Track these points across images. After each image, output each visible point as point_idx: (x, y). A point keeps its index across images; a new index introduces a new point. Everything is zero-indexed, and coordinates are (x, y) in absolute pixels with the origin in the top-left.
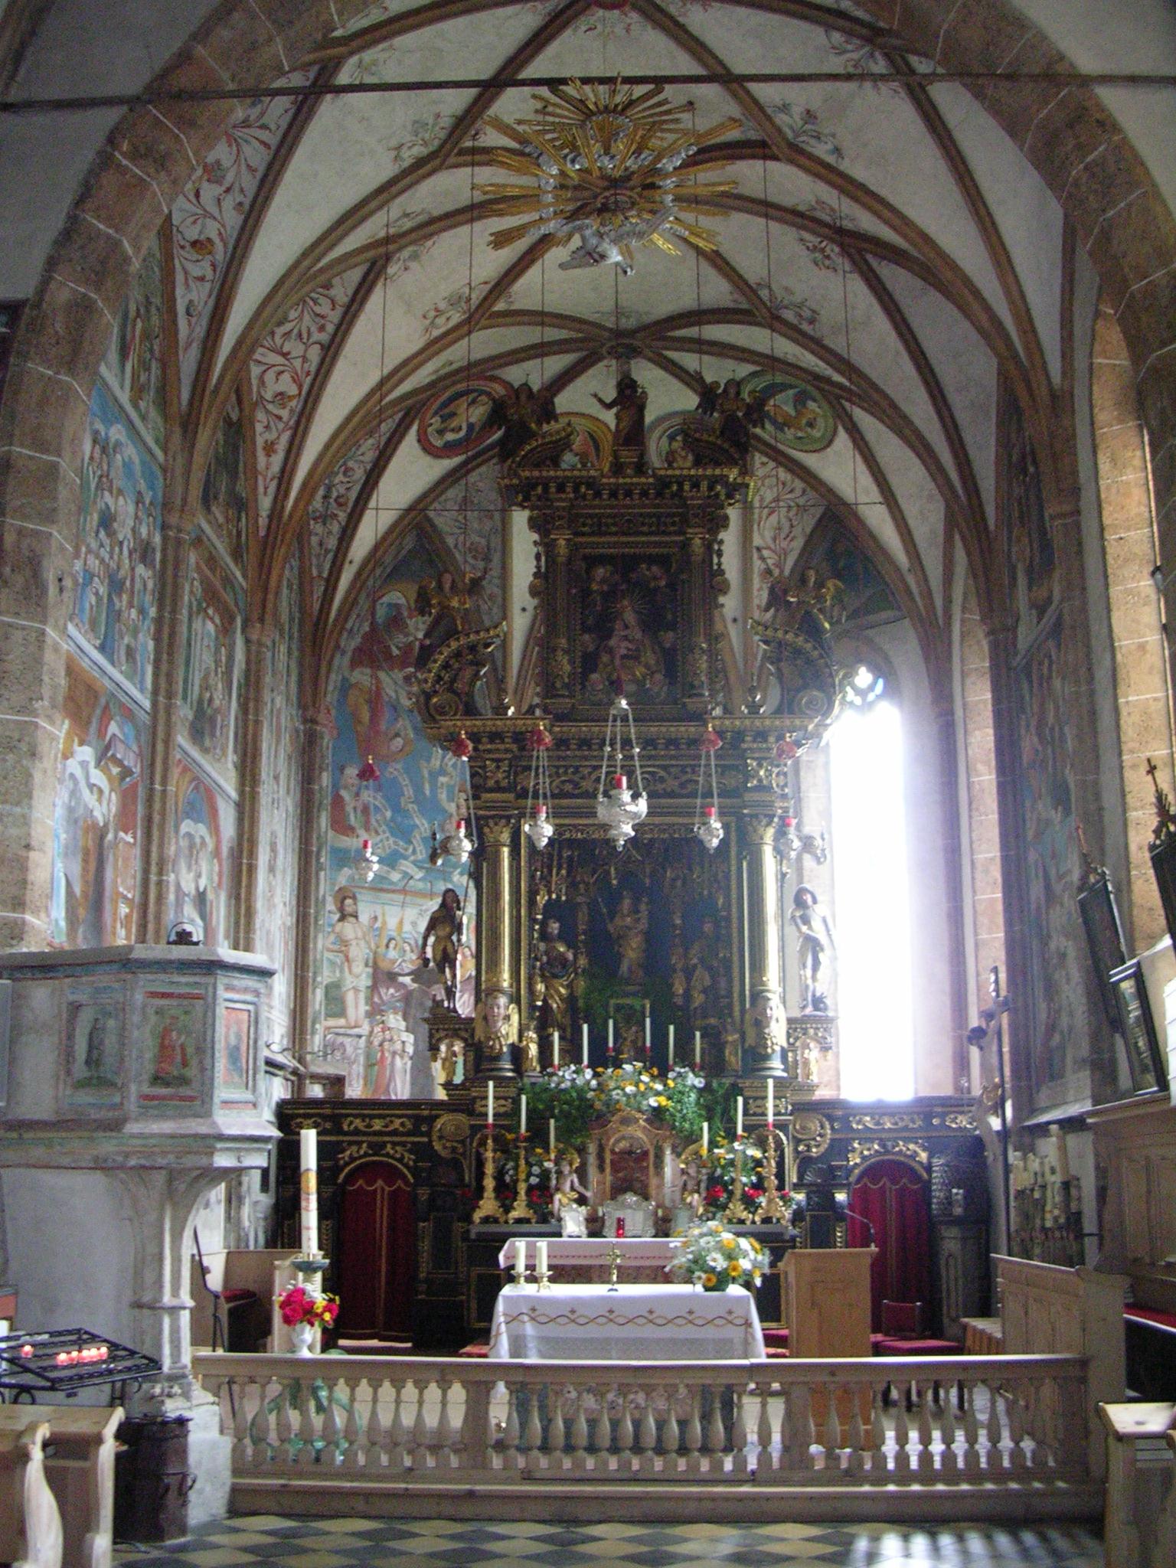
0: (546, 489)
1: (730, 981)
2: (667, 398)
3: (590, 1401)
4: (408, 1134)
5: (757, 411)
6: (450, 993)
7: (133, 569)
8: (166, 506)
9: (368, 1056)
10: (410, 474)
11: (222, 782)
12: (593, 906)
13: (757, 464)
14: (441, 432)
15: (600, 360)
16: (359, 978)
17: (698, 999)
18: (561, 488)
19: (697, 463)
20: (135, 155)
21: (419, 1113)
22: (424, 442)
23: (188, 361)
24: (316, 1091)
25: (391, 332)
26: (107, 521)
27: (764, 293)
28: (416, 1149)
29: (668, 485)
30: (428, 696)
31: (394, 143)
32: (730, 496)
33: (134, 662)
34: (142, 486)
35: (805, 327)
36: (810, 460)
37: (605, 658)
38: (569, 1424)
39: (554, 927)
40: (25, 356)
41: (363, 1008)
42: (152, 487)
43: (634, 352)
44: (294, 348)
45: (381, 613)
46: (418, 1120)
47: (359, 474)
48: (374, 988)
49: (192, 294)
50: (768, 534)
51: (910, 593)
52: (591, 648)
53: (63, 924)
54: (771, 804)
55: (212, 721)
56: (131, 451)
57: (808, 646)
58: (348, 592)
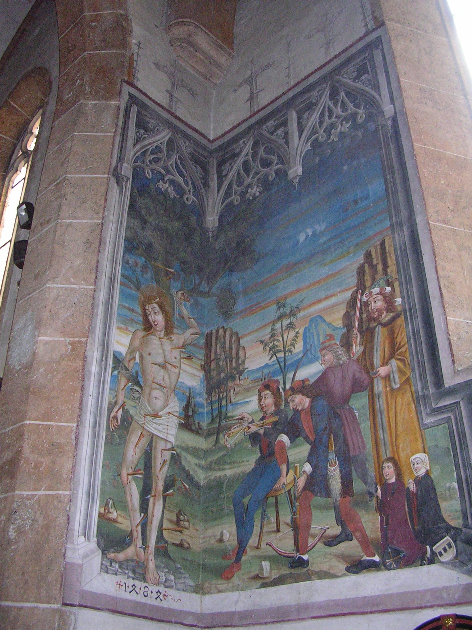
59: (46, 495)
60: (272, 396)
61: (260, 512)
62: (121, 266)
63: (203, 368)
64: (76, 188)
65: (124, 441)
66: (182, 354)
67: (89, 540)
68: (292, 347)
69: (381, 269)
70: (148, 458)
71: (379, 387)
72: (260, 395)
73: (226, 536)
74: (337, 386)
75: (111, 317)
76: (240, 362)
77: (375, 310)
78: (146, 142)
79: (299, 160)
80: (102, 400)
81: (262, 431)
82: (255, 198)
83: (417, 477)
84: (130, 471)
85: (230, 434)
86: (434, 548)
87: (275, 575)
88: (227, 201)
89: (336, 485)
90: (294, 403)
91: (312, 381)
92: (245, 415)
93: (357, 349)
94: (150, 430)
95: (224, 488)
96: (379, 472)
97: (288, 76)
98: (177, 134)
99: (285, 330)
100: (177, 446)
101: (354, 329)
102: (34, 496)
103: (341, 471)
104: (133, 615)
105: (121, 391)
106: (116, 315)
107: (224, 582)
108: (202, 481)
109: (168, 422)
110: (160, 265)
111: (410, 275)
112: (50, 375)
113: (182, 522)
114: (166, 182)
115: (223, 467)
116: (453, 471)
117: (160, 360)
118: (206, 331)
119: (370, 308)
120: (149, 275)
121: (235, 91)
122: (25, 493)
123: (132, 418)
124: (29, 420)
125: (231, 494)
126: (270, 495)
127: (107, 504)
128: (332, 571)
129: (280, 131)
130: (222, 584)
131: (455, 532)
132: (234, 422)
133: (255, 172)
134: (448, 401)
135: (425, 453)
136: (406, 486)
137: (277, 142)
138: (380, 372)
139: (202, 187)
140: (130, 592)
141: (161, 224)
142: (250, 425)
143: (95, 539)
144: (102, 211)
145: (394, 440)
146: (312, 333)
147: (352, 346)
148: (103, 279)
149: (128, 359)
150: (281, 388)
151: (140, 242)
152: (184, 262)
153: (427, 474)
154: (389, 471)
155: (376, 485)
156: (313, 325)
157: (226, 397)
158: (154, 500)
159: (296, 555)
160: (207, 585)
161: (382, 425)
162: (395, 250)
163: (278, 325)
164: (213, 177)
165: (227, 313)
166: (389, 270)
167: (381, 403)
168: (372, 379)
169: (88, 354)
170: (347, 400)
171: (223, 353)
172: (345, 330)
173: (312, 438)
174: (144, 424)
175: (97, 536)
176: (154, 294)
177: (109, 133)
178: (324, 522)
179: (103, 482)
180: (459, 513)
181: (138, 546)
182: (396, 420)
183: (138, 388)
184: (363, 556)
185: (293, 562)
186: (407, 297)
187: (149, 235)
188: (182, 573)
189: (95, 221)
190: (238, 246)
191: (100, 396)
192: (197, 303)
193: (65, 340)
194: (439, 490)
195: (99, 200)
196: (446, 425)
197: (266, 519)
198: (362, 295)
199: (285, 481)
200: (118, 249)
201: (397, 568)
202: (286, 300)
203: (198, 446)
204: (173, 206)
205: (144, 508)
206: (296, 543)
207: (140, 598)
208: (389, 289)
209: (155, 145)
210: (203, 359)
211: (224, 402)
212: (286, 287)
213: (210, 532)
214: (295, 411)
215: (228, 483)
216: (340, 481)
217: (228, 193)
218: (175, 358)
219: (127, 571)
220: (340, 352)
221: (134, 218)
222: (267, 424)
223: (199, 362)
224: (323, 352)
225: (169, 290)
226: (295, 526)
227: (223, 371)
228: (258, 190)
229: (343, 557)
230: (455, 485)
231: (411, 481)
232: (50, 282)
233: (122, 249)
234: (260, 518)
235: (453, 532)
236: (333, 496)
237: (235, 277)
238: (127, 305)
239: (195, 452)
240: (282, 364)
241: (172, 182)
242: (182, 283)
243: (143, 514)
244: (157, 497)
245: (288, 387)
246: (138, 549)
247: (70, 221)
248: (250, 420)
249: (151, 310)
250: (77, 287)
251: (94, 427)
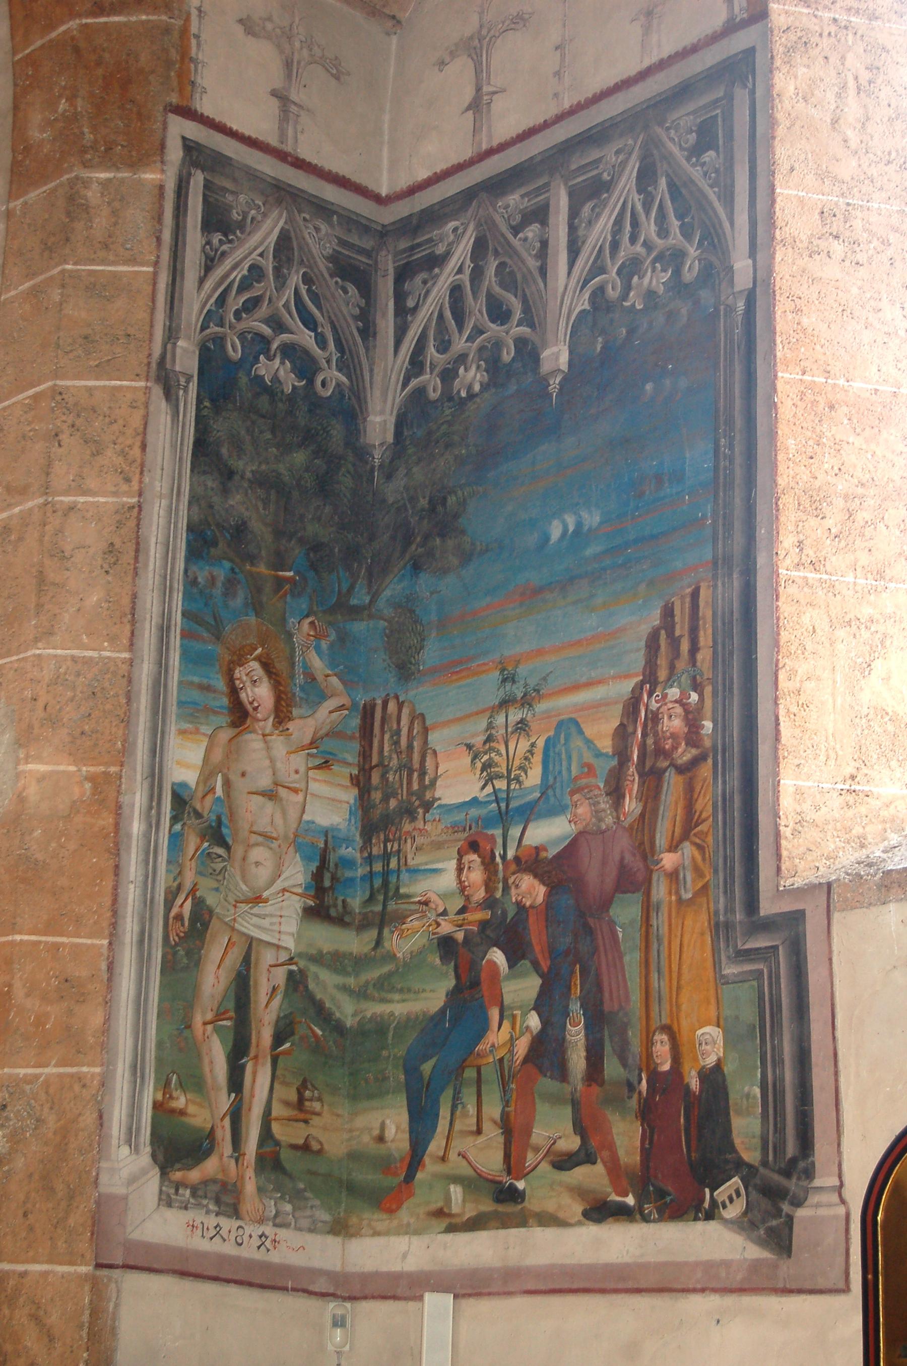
59: (61, 1076)
60: (482, 868)
61: (448, 1094)
62: (181, 595)
63: (355, 781)
64: (78, 416)
65: (195, 960)
66: (310, 759)
67: (137, 1151)
68: (522, 774)
69: (686, 651)
70: (242, 986)
71: (660, 890)
72: (460, 860)
73: (391, 1132)
74: (595, 872)
75: (164, 711)
76: (427, 782)
77: (668, 734)
78: (228, 263)
79: (563, 329)
80: (153, 888)
81: (460, 936)
82: (471, 396)
83: (704, 1067)
84: (209, 1016)
85: (403, 931)
86: (715, 1194)
87: (470, 1212)
88: (414, 383)
89: (578, 1060)
90: (519, 891)
91: (552, 852)
92: (434, 898)
93: (631, 805)
94: (245, 931)
95: (390, 1038)
96: (647, 1049)
97: (557, 74)
98: (300, 212)
99: (512, 733)
100: (300, 955)
101: (630, 764)
102: (37, 1077)
103: (587, 1036)
104: (215, 1279)
105: (188, 863)
106: (174, 708)
107: (385, 1216)
108: (350, 1018)
109: (281, 908)
110: (262, 569)
111: (732, 679)
112: (54, 845)
113: (307, 1103)
114: (275, 355)
115: (389, 996)
116: (756, 1068)
117: (265, 782)
118: (362, 699)
119: (660, 726)
120: (238, 601)
121: (442, 64)
122: (22, 1072)
123: (211, 912)
124: (20, 933)
125: (400, 1051)
126: (467, 1063)
127: (167, 1083)
128: (561, 1215)
129: (532, 232)
130: (380, 1220)
131: (749, 1173)
132: (413, 907)
133: (475, 327)
134: (761, 942)
135: (718, 1026)
136: (686, 1082)
137: (523, 261)
138: (664, 862)
139: (359, 340)
140: (211, 1238)
141: (263, 467)
142: (440, 919)
143: (148, 1149)
144: (137, 476)
145: (674, 996)
146: (559, 754)
147: (624, 797)
148: (147, 633)
149: (200, 794)
150: (497, 854)
151: (218, 525)
152: (316, 547)
153: (718, 1066)
154: (662, 1048)
155: (641, 1070)
156: (562, 736)
157: (399, 851)
158: (256, 1065)
159: (507, 1180)
160: (354, 1220)
161: (659, 963)
162: (714, 614)
163: (500, 720)
164: (387, 305)
165: (405, 670)
166: (699, 657)
167: (660, 922)
168: (650, 872)
169: (125, 799)
170: (606, 904)
171: (395, 756)
172: (614, 762)
173: (545, 965)
174: (235, 920)
175: (152, 1143)
176: (252, 640)
177: (142, 265)
178: (554, 1128)
179: (160, 1045)
180: (757, 1141)
181: (225, 1155)
182: (680, 959)
183: (220, 851)
184: (609, 1194)
185: (501, 1191)
186: (722, 725)
187: (240, 504)
188: (306, 1199)
189: (125, 499)
190: (433, 509)
191: (149, 878)
192: (343, 638)
193: (79, 770)
194: (733, 1097)
195: (130, 447)
196: (755, 983)
197: (460, 1107)
198: (650, 695)
199: (495, 1041)
200: (174, 558)
201: (660, 1220)
202: (517, 667)
203: (343, 948)
204: (291, 411)
205: (236, 1083)
206: (507, 1157)
207: (229, 1249)
208: (694, 697)
209: (246, 265)
210: (356, 761)
211: (393, 864)
212: (520, 637)
213: (360, 1122)
214: (520, 905)
215: (395, 1028)
216: (585, 1054)
217: (416, 364)
218: (297, 772)
219: (205, 1202)
220: (603, 806)
221: (205, 473)
222: (470, 923)
223: (343, 772)
224: (576, 797)
225: (284, 620)
226: (506, 1126)
227: (394, 794)
228: (478, 375)
229: (580, 1192)
230: (757, 1091)
231: (694, 1073)
232: (40, 645)
233: (183, 554)
234: (450, 1105)
235: (745, 1171)
236: (571, 1079)
237: (424, 582)
238: (196, 679)
239: (336, 961)
240: (503, 805)
241: (289, 351)
242: (311, 599)
243: (233, 1095)
244: (261, 1061)
245: (510, 854)
246: (225, 1159)
247: (72, 499)
248: (441, 910)
249: (244, 678)
250: (94, 654)
251: (141, 942)
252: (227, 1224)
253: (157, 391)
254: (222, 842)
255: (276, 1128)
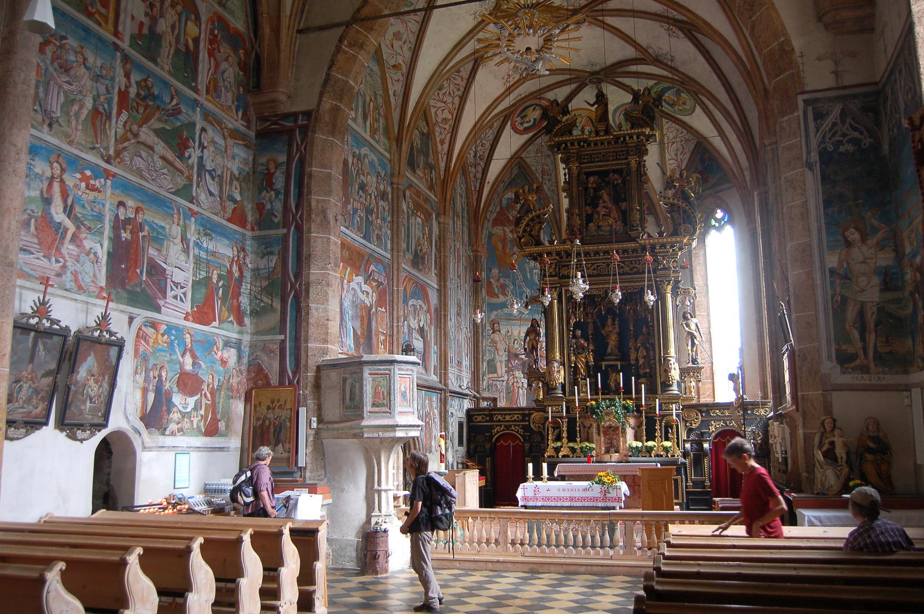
0: (566, 145)
1: (655, 354)
2: (617, 98)
3: (555, 527)
4: (521, 421)
5: (658, 100)
6: (536, 362)
7: (377, 204)
8: (392, 175)
9: (507, 389)
10: (510, 143)
11: (429, 282)
12: (594, 323)
13: (664, 123)
14: (522, 124)
15: (587, 85)
16: (502, 357)
17: (641, 361)
18: (572, 144)
19: (632, 128)
20: (350, 46)
21: (525, 414)
22: (514, 128)
23: (396, 115)
24: (484, 404)
25: (489, 86)
26: (363, 187)
27: (650, 50)
28: (524, 427)
29: (619, 138)
30: (520, 239)
31: (472, 12)
32: (647, 140)
33: (381, 240)
34: (380, 169)
35: (669, 63)
36: (686, 119)
37: (596, 216)
38: (548, 536)
39: (579, 333)
40: (314, 132)
41: (504, 369)
42: (384, 169)
43: (600, 81)
44: (449, 100)
45: (504, 202)
46: (524, 415)
47: (488, 146)
48: (509, 361)
49: (395, 88)
50: (673, 153)
51: (734, 173)
52: (590, 212)
53: (352, 346)
54: (669, 276)
55: (423, 258)
56: (372, 157)
57: (684, 205)
58: (488, 195)
117: (861, 259)
179: (835, 334)
205: (863, 339)
252: (867, 376)
253: (807, 170)
254: (849, 279)
255: (879, 349)
